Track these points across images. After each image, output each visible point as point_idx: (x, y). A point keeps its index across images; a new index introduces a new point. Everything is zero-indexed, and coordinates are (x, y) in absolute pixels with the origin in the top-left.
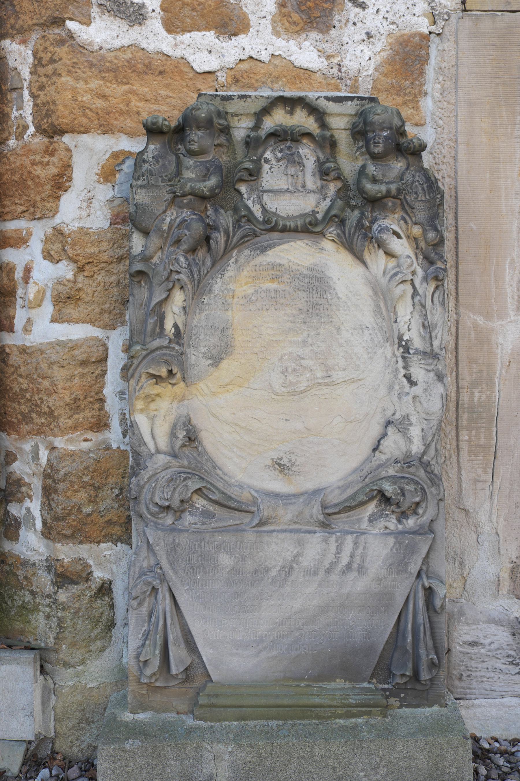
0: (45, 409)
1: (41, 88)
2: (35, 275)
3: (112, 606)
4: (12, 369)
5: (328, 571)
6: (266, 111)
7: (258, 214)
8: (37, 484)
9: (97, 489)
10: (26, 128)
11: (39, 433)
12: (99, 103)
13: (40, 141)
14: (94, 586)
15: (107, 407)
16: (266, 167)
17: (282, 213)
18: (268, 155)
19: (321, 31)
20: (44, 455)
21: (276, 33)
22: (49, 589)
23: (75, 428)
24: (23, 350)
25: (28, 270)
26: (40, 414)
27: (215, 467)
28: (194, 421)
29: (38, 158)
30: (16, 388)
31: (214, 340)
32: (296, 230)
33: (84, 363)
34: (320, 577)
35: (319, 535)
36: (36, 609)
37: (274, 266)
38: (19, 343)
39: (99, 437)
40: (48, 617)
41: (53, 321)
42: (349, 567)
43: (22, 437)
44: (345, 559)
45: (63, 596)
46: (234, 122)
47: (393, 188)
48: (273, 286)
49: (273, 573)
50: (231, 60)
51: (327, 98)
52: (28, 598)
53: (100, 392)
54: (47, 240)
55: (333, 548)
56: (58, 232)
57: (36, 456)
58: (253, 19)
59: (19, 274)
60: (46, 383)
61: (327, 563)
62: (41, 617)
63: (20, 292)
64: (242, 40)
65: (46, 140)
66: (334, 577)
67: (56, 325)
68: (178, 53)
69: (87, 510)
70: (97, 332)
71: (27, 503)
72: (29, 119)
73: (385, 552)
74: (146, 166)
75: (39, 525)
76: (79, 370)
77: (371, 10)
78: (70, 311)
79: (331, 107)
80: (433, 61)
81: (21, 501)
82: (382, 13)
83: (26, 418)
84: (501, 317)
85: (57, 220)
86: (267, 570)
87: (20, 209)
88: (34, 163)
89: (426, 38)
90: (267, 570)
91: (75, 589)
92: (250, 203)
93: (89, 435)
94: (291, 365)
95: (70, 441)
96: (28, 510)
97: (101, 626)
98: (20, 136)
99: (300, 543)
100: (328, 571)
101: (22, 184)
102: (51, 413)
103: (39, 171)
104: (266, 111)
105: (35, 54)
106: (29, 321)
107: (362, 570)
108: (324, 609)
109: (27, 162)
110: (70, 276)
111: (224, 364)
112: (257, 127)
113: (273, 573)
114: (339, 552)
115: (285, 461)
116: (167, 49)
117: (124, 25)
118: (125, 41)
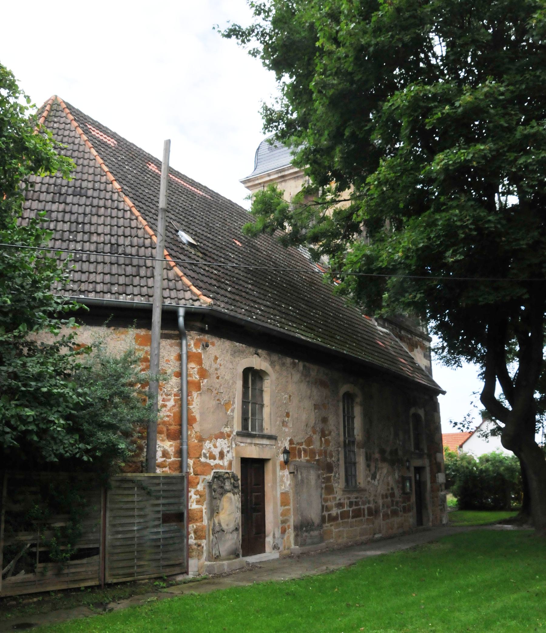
20: (195, 527)
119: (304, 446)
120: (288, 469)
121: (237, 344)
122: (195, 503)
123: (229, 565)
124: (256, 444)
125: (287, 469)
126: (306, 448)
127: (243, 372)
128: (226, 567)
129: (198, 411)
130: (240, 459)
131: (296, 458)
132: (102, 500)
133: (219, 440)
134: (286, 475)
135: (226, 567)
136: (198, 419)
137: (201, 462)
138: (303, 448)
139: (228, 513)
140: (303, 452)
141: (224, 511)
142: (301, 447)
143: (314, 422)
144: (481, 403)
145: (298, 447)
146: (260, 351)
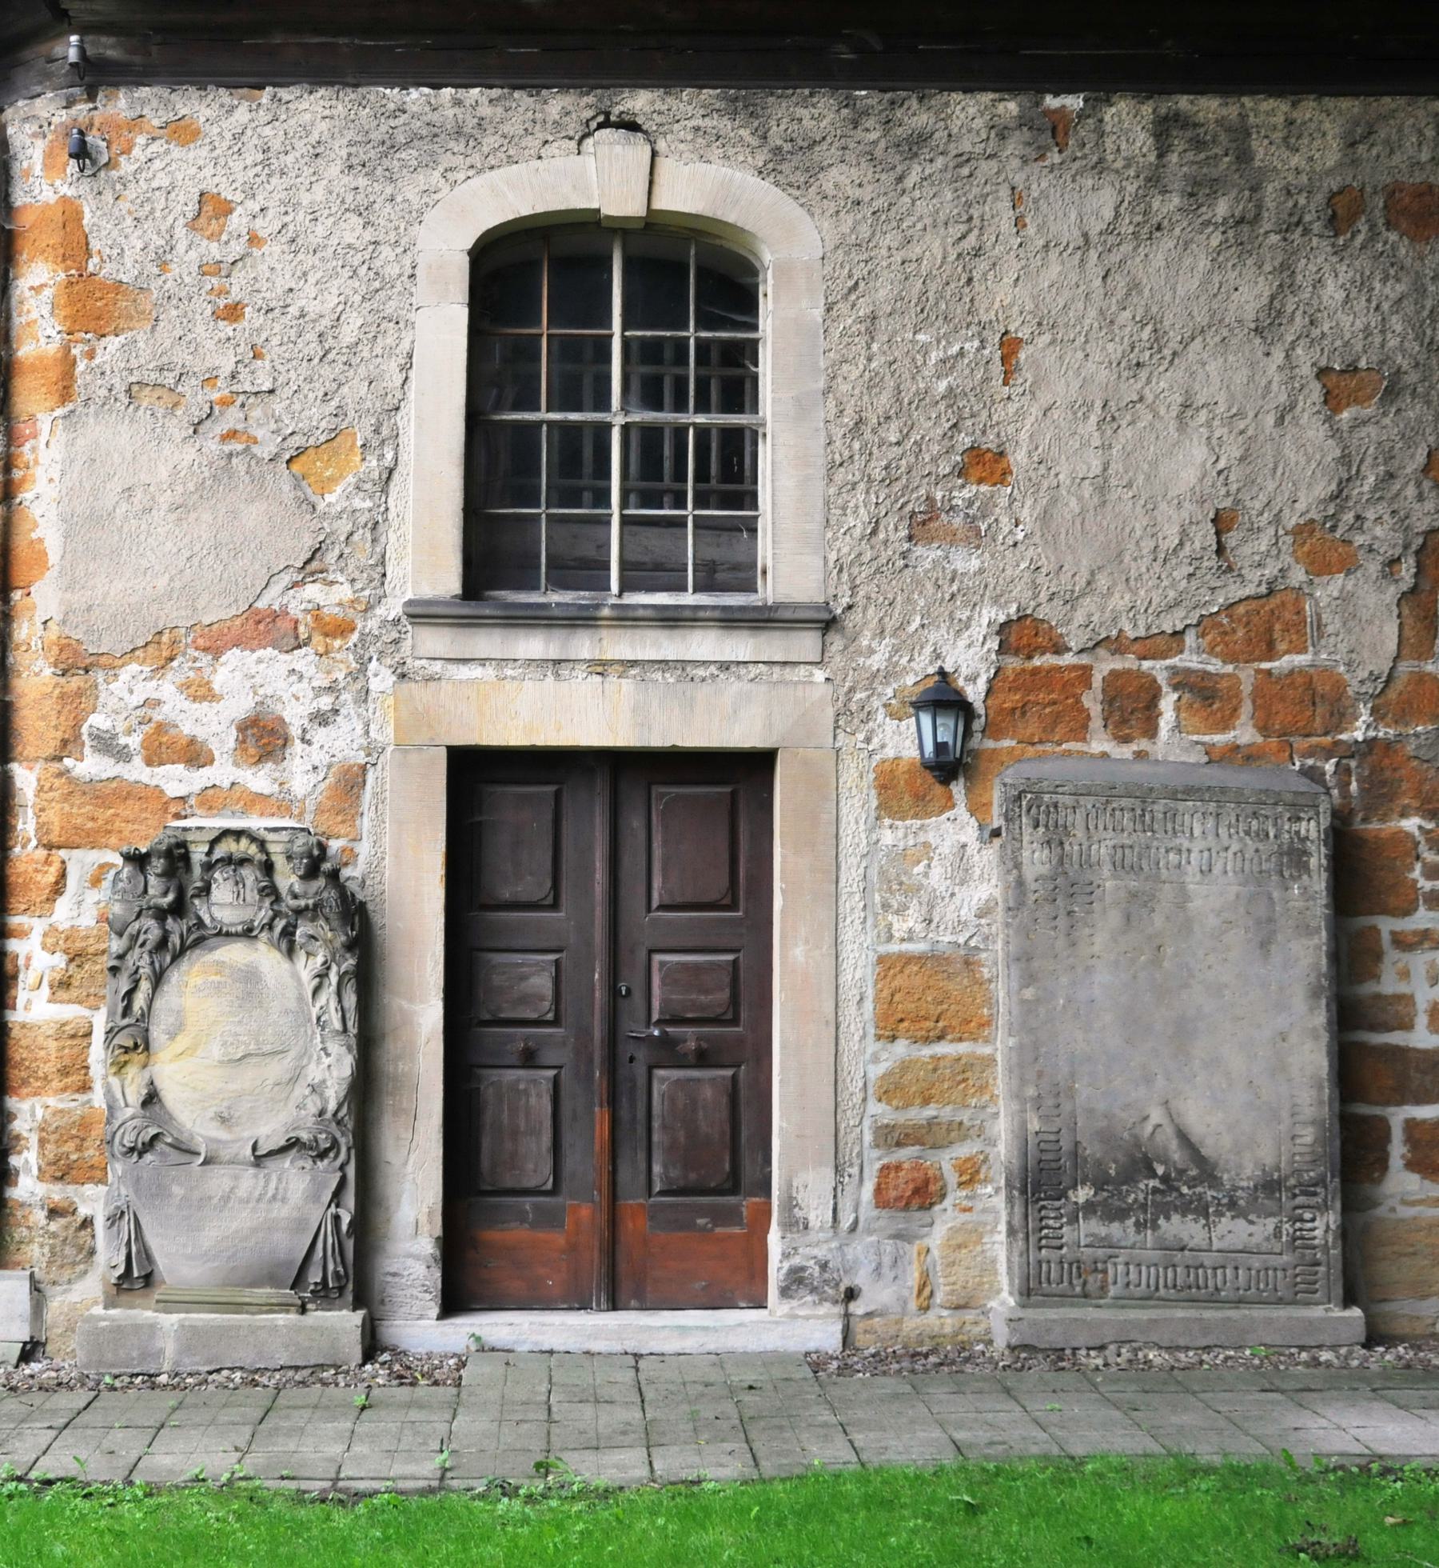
0: (40, 1074)
1: (42, 810)
2: (34, 963)
3: (93, 1236)
4: (1218, 649)
5: (259, 1200)
6: (213, 843)
7: (207, 920)
8: (34, 1139)
9: (83, 1140)
10: (29, 840)
11: (35, 1094)
12: (90, 825)
13: (42, 853)
14: (79, 1220)
15: (91, 1072)
16: (214, 886)
17: (226, 920)
18: (217, 875)
19: (276, 763)
20: (39, 1113)
21: (236, 764)
22: (44, 1222)
23: (64, 1090)
24: (23, 1026)
25: (28, 959)
26: (37, 1079)
27: (171, 1118)
28: (156, 1083)
29: (39, 866)
30: (18, 1058)
31: (171, 1020)
32: (237, 935)
33: (73, 1037)
34: (251, 1205)
35: (252, 1171)
36: (31, 1241)
37: (218, 963)
38: (20, 1019)
39: (82, 1098)
40: (42, 1246)
41: (49, 1001)
42: (274, 1197)
43: (22, 1099)
44: (270, 1194)
45: (54, 1227)
46: (192, 848)
47: (311, 902)
48: (218, 978)
49: (215, 1201)
50: (196, 788)
51: (266, 829)
52: (25, 1232)
53: (85, 1060)
54: (45, 935)
55: (262, 1183)
56: (53, 929)
57: (33, 1114)
58: (217, 754)
59: (21, 962)
60: (42, 1053)
61: (257, 1194)
62: (35, 1247)
63: (21, 977)
64: (205, 771)
65: (46, 852)
66: (262, 1205)
67: (51, 1005)
68: (154, 783)
69: (74, 1157)
70: (87, 1013)
71: (25, 1154)
72: (32, 833)
73: (302, 1187)
74: (121, 885)
75: (35, 1171)
76: (69, 1042)
77: (316, 746)
78: (62, 994)
79: (270, 837)
80: (368, 787)
81: (20, 1153)
82: (326, 748)
83: (25, 1082)
84: (422, 1002)
85: (54, 918)
86: (210, 1198)
87: (23, 907)
88: (37, 871)
89: (364, 769)
90: (210, 1198)
91: (62, 1221)
92: (201, 913)
93: (76, 1096)
94: (231, 1039)
95: (62, 1100)
96: (27, 1161)
97: (84, 1252)
98: (24, 847)
99: (236, 1178)
100: (259, 1200)
101: (26, 885)
102: (46, 1078)
103: (39, 877)
104: (213, 843)
105: (39, 780)
106: (29, 1001)
107: (284, 1200)
108: (254, 1230)
109: (30, 869)
110: (63, 965)
111: (179, 1038)
112: (209, 853)
113: (215, 1201)
114: (266, 1186)
115: (226, 1115)
116: (145, 779)
117: (112, 761)
118: (111, 774)
119: (1189, 659)
120: (977, 809)
121: (416, 96)
122: (45, 990)
123: (191, 1338)
124: (600, 667)
125: (961, 811)
126: (1215, 666)
127: (470, 253)
128: (170, 1348)
129: (53, 513)
130: (443, 752)
131: (1080, 731)
132: (518, 958)
133: (233, 656)
134: (946, 848)
135: (170, 1348)
136: (53, 558)
137: (72, 781)
138: (1174, 671)
139: (216, 1052)
140: (1167, 704)
141: (182, 1042)
142: (1157, 669)
143: (1323, 488)
144: (484, 229)
145: (1105, 665)
146: (639, 102)
